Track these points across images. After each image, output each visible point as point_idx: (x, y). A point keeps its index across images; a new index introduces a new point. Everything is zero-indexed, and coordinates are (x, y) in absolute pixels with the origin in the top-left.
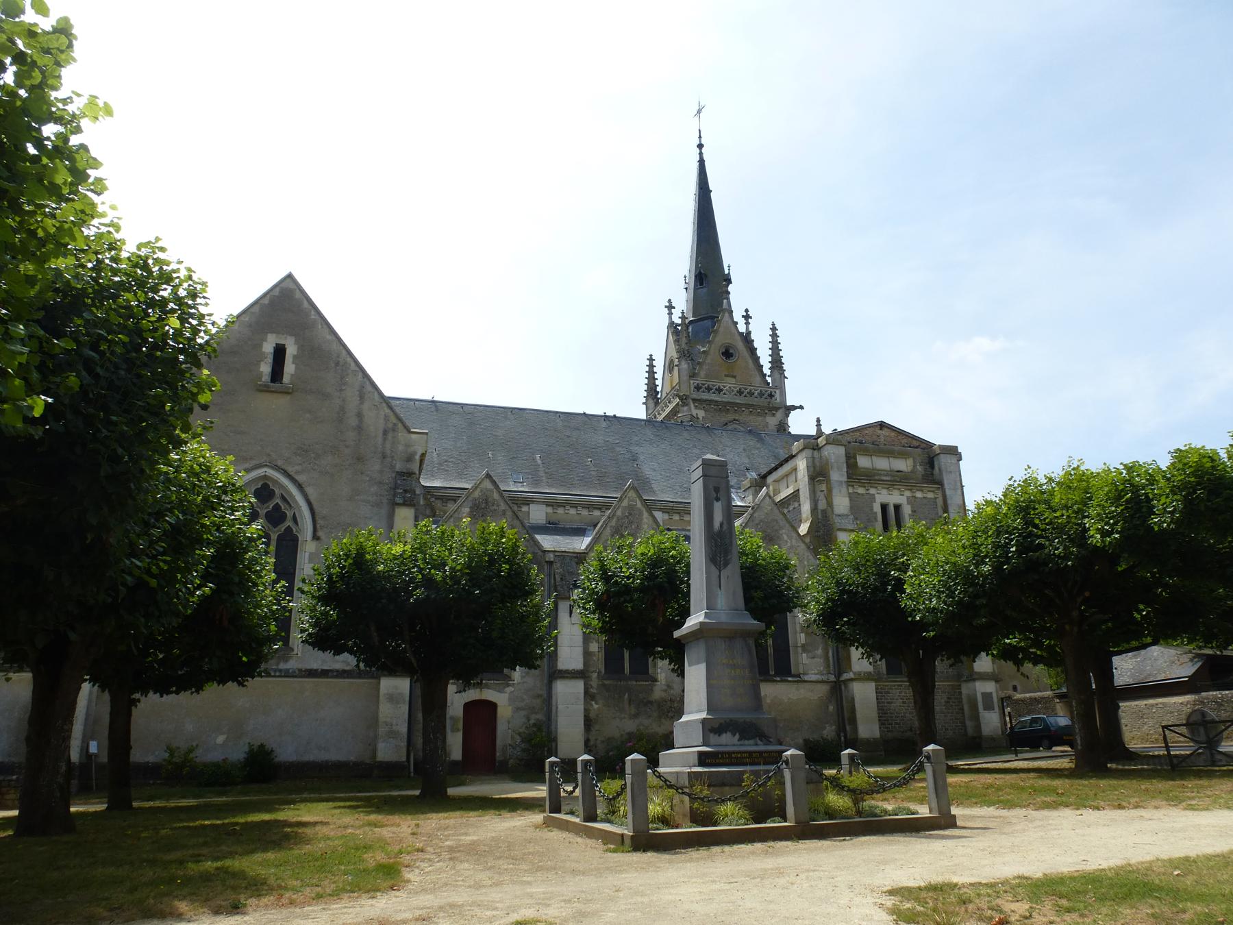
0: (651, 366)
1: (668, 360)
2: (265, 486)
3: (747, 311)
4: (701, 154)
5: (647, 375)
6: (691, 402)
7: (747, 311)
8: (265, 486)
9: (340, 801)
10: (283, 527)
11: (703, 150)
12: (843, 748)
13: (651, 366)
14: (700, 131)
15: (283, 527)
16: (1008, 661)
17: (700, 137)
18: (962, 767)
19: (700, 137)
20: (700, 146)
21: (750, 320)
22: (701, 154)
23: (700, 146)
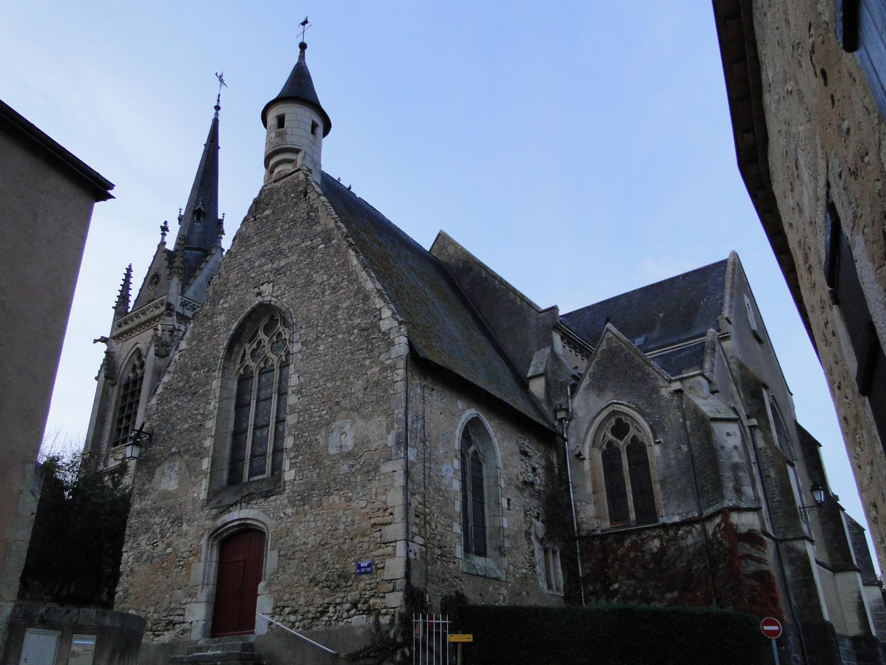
0: (128, 275)
1: (151, 274)
2: (619, 421)
3: (166, 223)
4: (217, 114)
5: (122, 282)
6: (175, 315)
7: (166, 223)
8: (619, 421)
9: (549, 567)
10: (628, 438)
11: (219, 112)
12: (858, 557)
13: (128, 275)
14: (219, 95)
15: (628, 438)
16: (453, 594)
17: (218, 101)
18: (794, 603)
19: (218, 101)
20: (217, 108)
21: (166, 232)
22: (217, 114)
23: (217, 108)
